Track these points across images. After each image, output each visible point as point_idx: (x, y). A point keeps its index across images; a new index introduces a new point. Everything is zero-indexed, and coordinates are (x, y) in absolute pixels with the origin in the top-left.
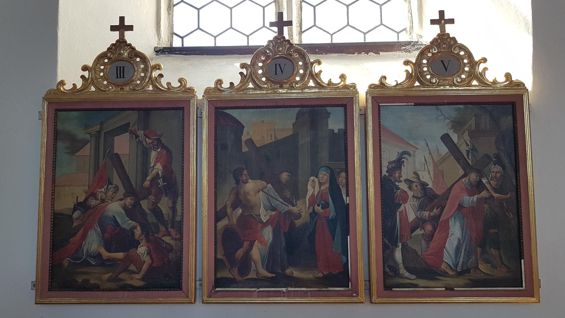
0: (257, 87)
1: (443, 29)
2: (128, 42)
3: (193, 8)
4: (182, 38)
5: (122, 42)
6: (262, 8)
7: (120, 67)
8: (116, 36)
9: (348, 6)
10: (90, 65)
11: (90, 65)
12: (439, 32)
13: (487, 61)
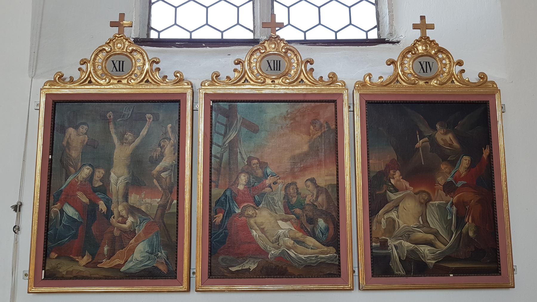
1: (424, 33)
2: (281, 38)
3: (168, 5)
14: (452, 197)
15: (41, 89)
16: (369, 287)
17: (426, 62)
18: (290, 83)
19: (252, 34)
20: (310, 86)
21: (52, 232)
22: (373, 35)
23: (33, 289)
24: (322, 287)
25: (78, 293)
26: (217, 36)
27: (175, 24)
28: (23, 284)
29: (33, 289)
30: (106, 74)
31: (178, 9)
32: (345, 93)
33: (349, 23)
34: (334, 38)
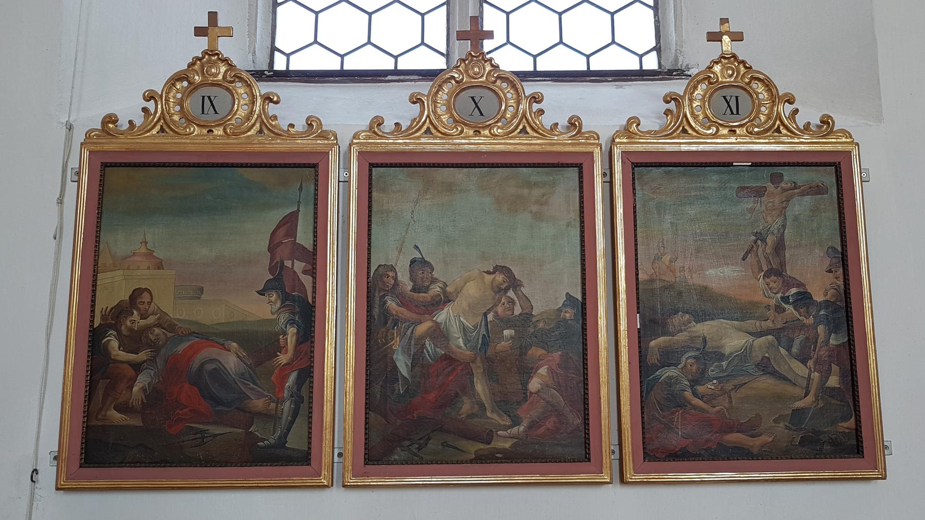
4: (288, 56)
5: (212, 52)
6: (505, 15)
8: (202, 43)
9: (612, 14)
14: (567, 321)
15: (82, 144)
16: (73, 484)
18: (758, 133)
19: (443, 60)
20: (441, 138)
22: (650, 62)
23: (351, 481)
25: (786, 483)
26: (333, 64)
27: (369, 42)
28: (48, 474)
29: (351, 481)
30: (708, 122)
32: (597, 151)
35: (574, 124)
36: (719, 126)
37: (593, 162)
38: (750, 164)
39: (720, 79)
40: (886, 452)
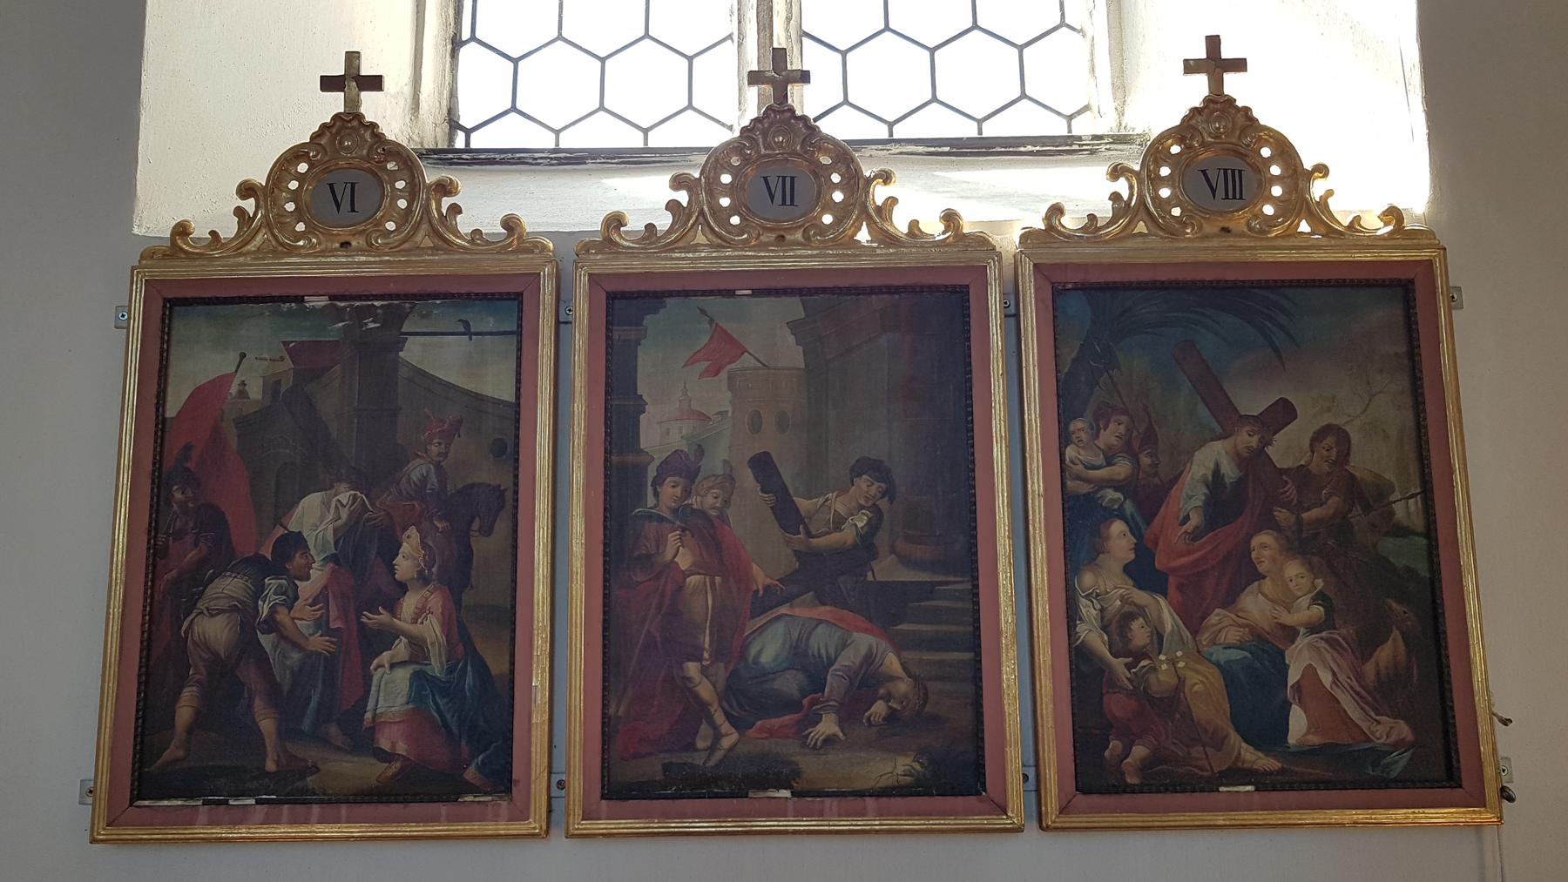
0: (722, 242)
1: (1216, 84)
7: (1233, 171)
8: (335, 103)
10: (261, 179)
11: (261, 179)
12: (1206, 92)
13: (240, 185)
15: (133, 268)
17: (1225, 171)
21: (1370, 768)
24: (578, 653)
31: (557, 128)
32: (992, 273)
33: (929, 97)
34: (975, 134)
35: (510, 224)
36: (1203, 221)
37: (985, 284)
38: (749, 292)
39: (763, 151)
40: (92, 784)
